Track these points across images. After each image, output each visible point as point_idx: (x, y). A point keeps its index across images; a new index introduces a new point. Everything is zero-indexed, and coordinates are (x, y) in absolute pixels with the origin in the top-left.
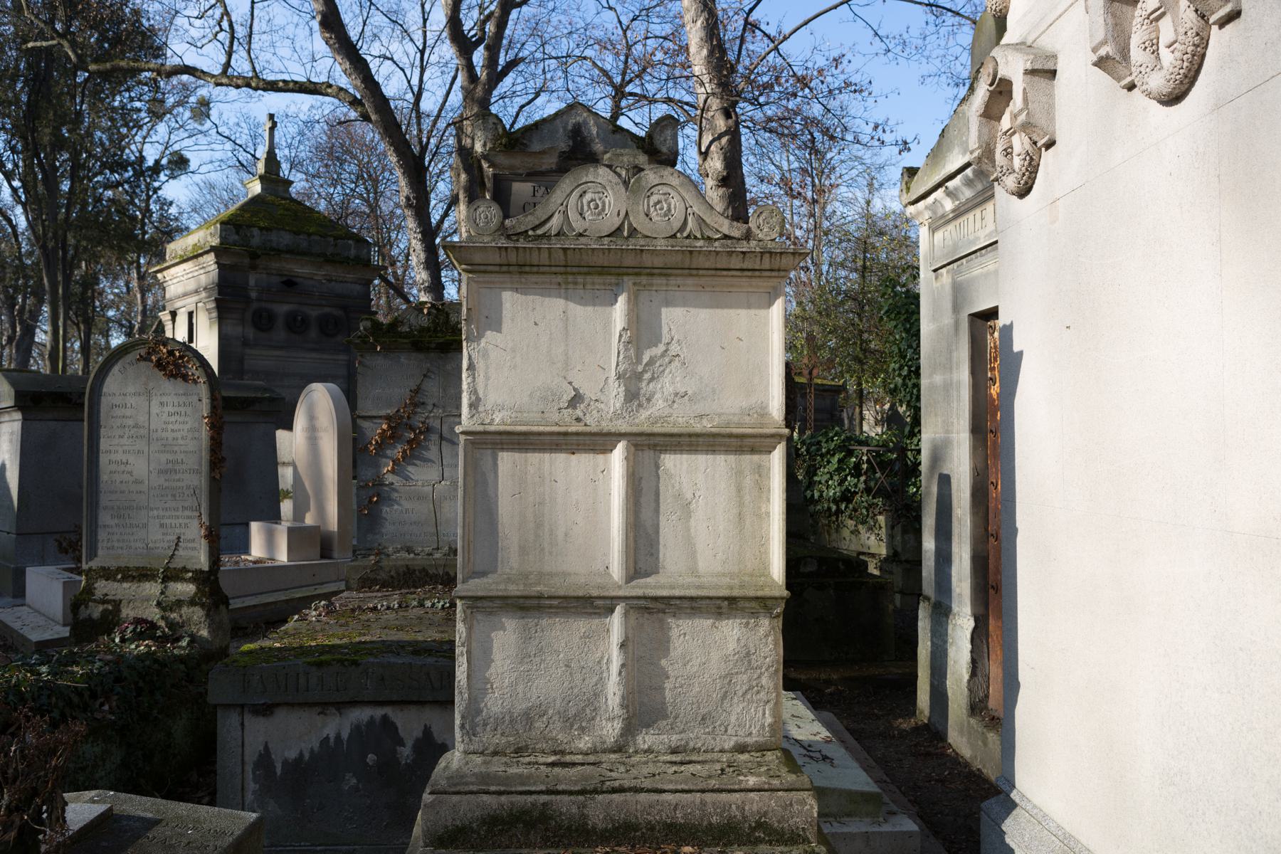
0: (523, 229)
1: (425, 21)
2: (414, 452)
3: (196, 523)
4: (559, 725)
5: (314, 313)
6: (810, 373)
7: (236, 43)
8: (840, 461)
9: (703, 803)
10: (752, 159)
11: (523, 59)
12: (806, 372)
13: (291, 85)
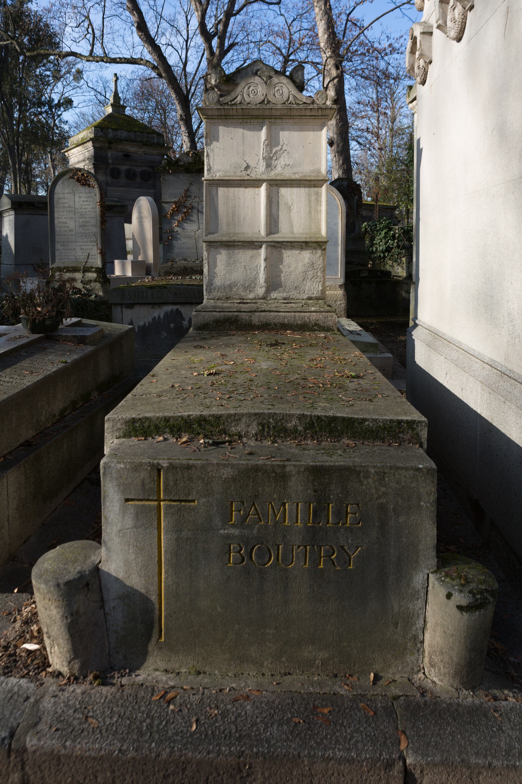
0: (226, 101)
1: (188, 25)
2: (187, 218)
3: (95, 248)
4: (242, 289)
5: (138, 170)
7: (95, 40)
8: (386, 233)
9: (295, 316)
11: (237, 43)
13: (123, 60)
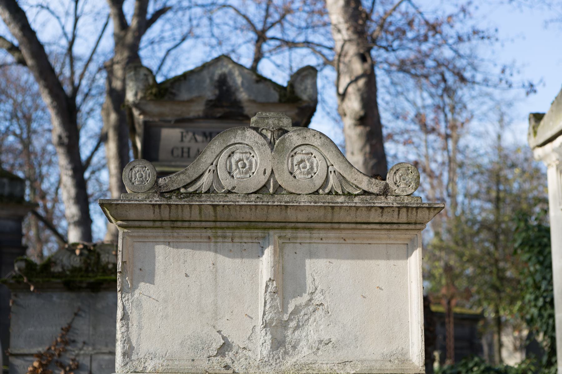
0: (175, 187)
6: (449, 303)
10: (388, 98)
12: (444, 302)
